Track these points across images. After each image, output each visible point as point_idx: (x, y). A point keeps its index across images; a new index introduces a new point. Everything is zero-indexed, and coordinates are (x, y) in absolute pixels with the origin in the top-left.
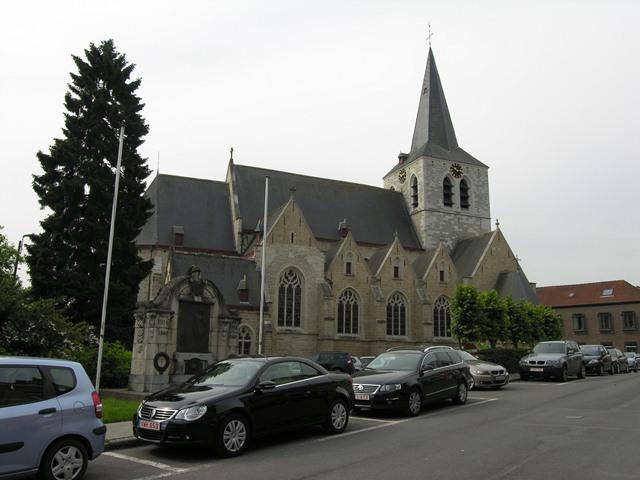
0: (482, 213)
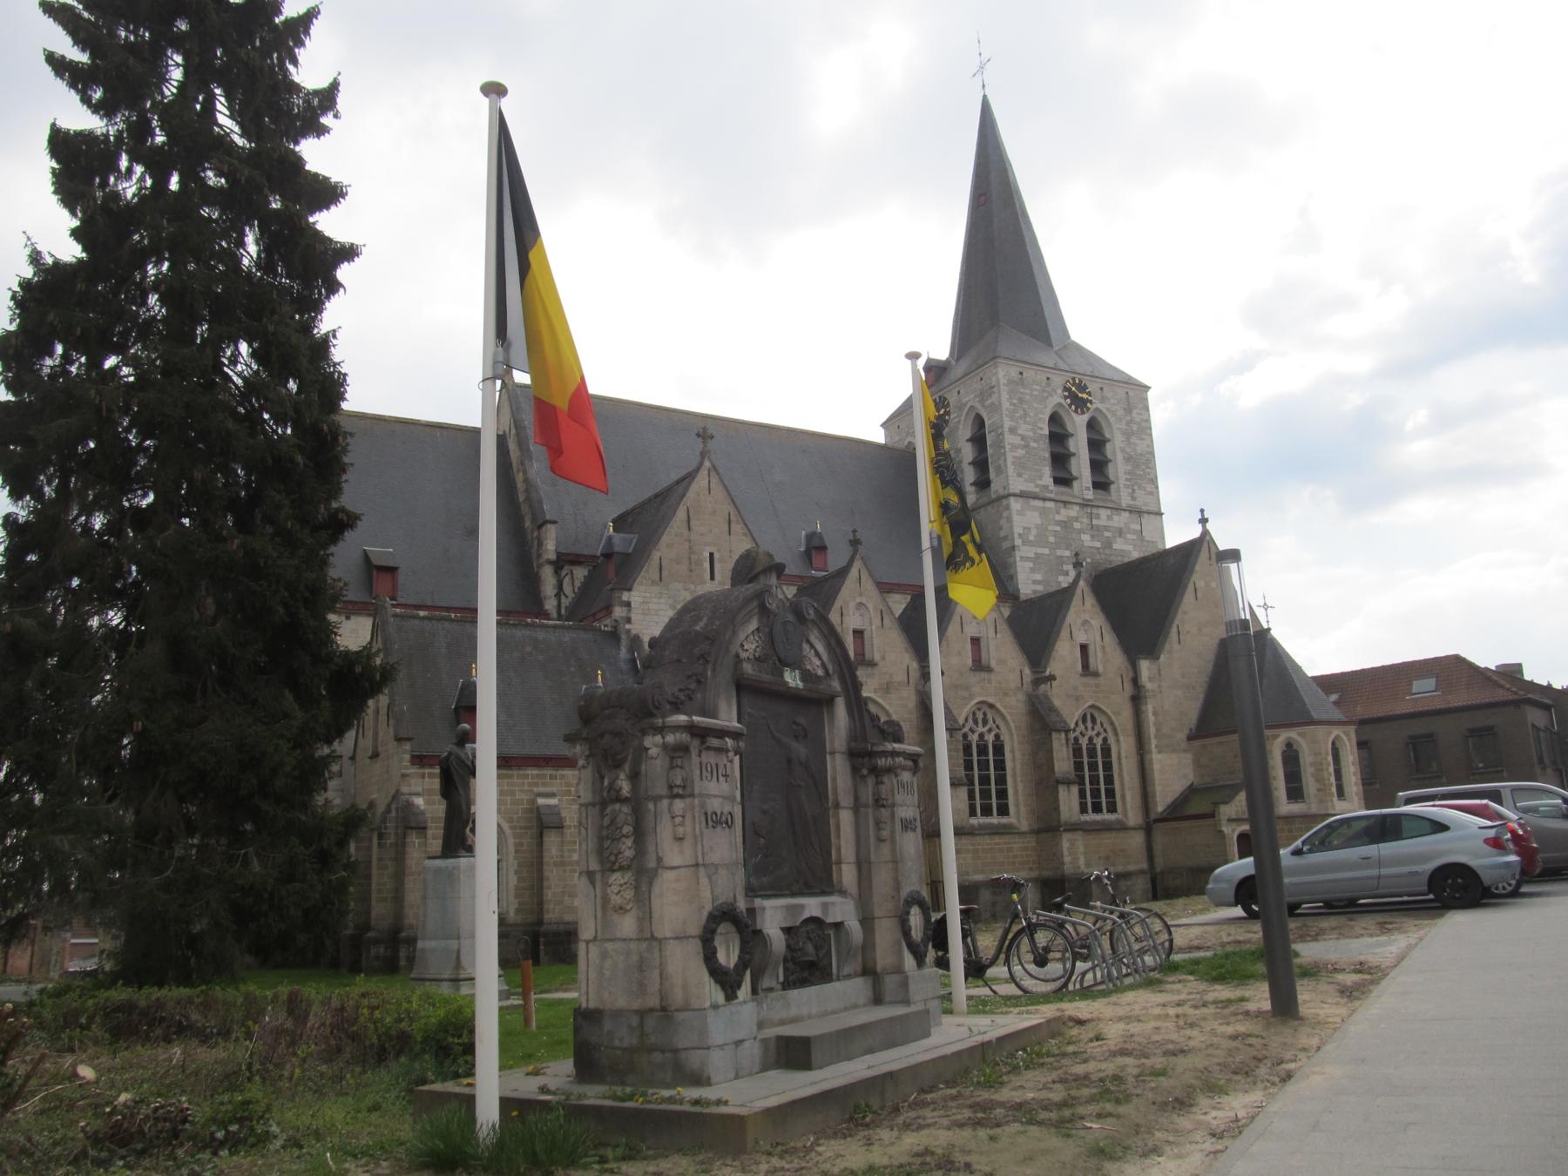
0: (1142, 501)
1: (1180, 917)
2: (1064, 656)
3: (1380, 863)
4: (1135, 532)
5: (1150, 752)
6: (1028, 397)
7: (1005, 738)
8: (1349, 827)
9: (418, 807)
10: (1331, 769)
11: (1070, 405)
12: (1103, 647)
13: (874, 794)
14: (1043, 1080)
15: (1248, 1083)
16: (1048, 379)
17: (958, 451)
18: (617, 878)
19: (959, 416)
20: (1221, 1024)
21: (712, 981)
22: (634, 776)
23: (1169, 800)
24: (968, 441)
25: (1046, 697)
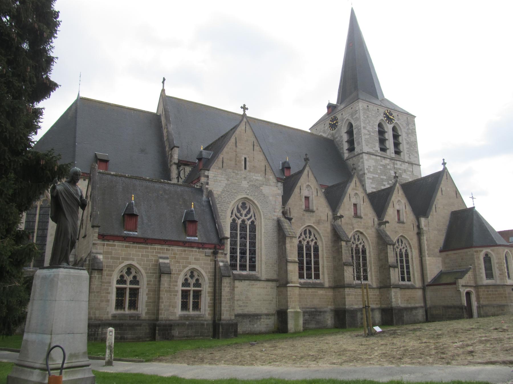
0: (412, 160)
2: (390, 214)
4: (410, 171)
5: (425, 256)
6: (370, 115)
7: (367, 247)
9: (100, 260)
10: (505, 266)
11: (386, 120)
12: (406, 212)
16: (378, 109)
17: (341, 137)
23: (433, 277)
24: (345, 133)
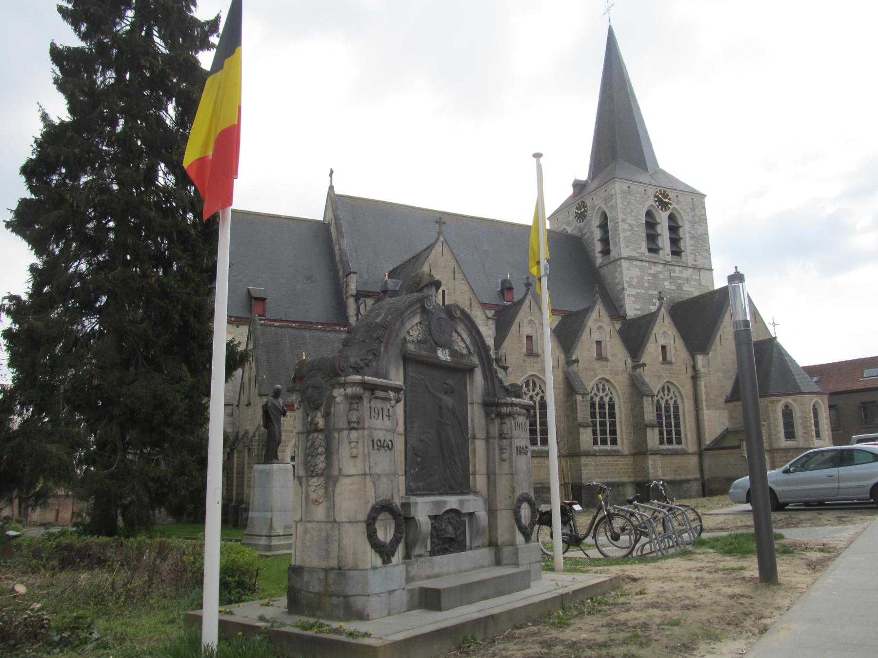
0: (700, 262)
1: (714, 509)
2: (651, 352)
3: (839, 479)
4: (696, 280)
5: (702, 409)
6: (633, 201)
7: (616, 399)
8: (823, 456)
10: (812, 421)
11: (658, 206)
12: (675, 347)
13: (499, 431)
14: (596, 623)
15: (737, 633)
16: (645, 190)
17: (592, 233)
18: (314, 481)
19: (593, 212)
20: (725, 586)
21: (373, 551)
22: (327, 415)
23: (714, 437)
24: (597, 227)
25: (641, 376)
